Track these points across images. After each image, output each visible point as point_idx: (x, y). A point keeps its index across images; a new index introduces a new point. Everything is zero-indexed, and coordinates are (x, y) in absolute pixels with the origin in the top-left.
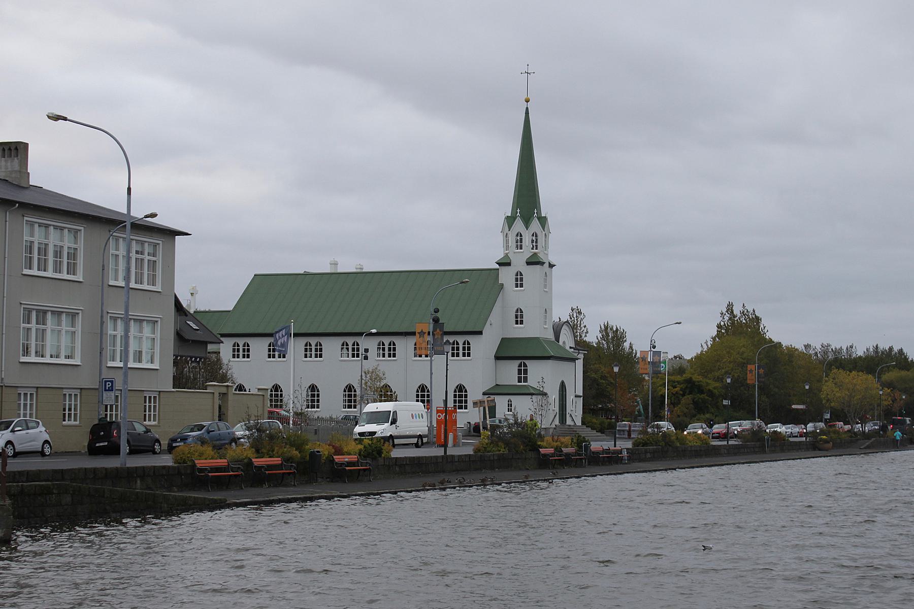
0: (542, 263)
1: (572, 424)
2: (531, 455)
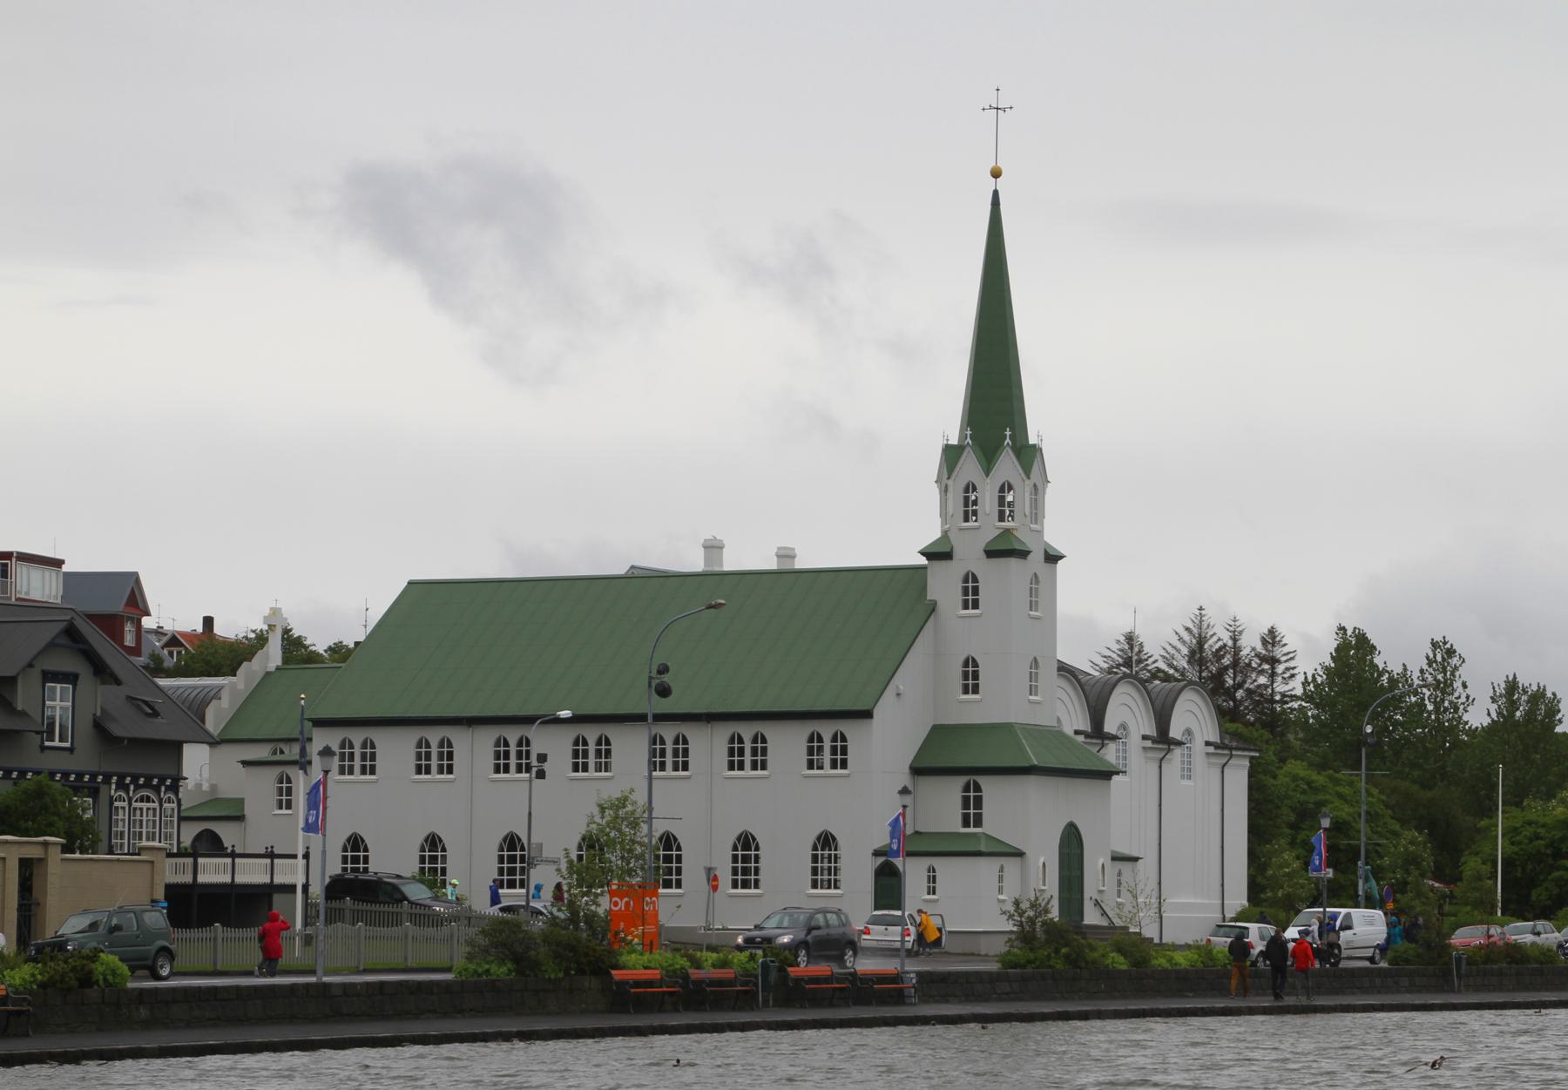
0: (1023, 554)
1: (1105, 923)
2: (591, 983)
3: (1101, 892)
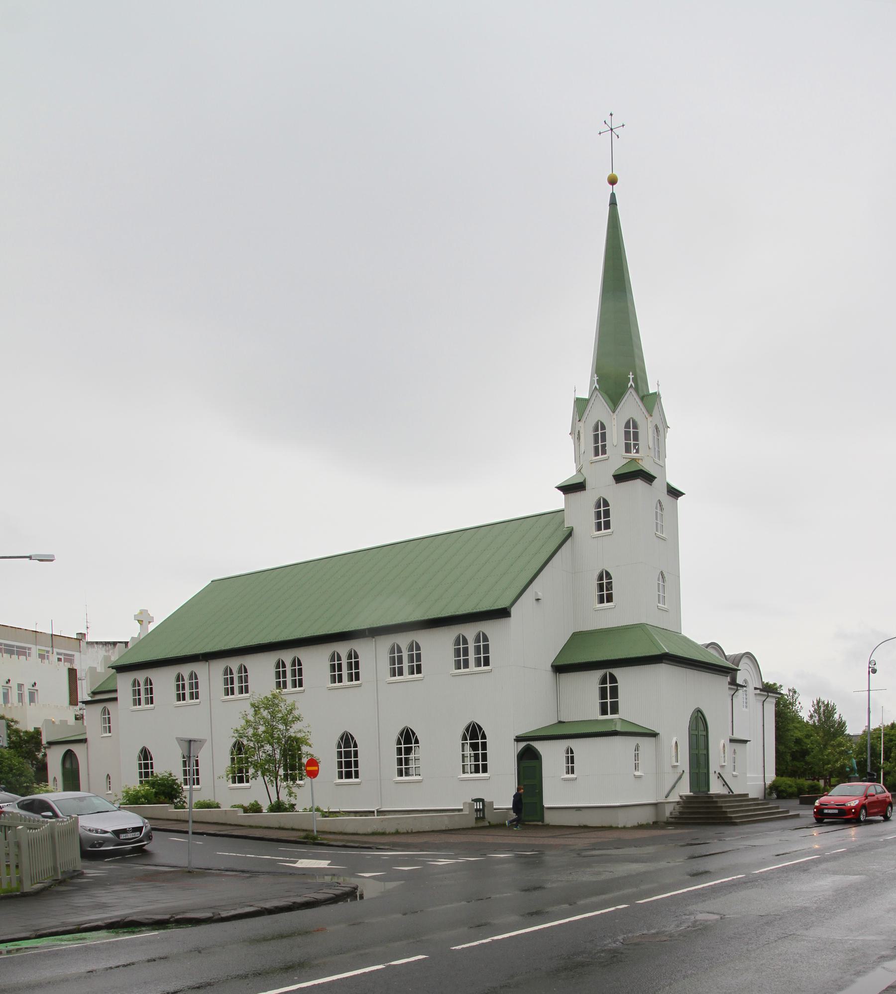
1: (725, 791)
3: (722, 766)
